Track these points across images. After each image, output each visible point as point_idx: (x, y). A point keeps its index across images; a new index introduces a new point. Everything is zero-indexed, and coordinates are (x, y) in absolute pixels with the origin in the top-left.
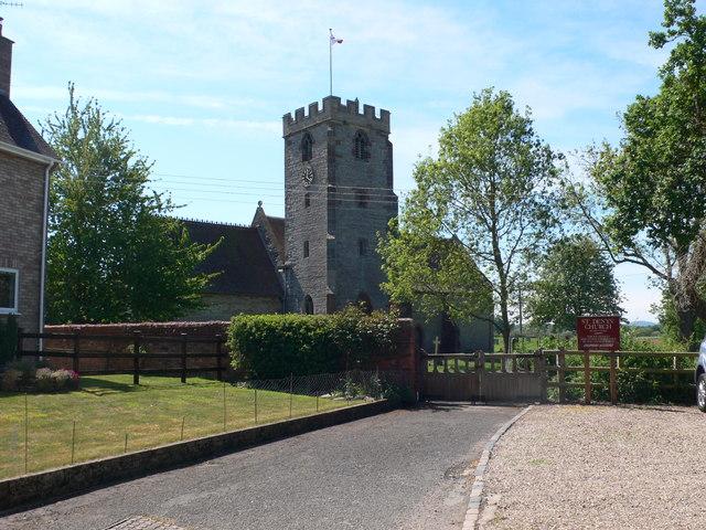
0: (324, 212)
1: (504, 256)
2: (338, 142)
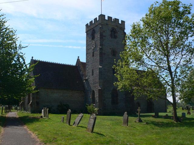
0: (98, 58)
1: (173, 69)
2: (104, 31)
